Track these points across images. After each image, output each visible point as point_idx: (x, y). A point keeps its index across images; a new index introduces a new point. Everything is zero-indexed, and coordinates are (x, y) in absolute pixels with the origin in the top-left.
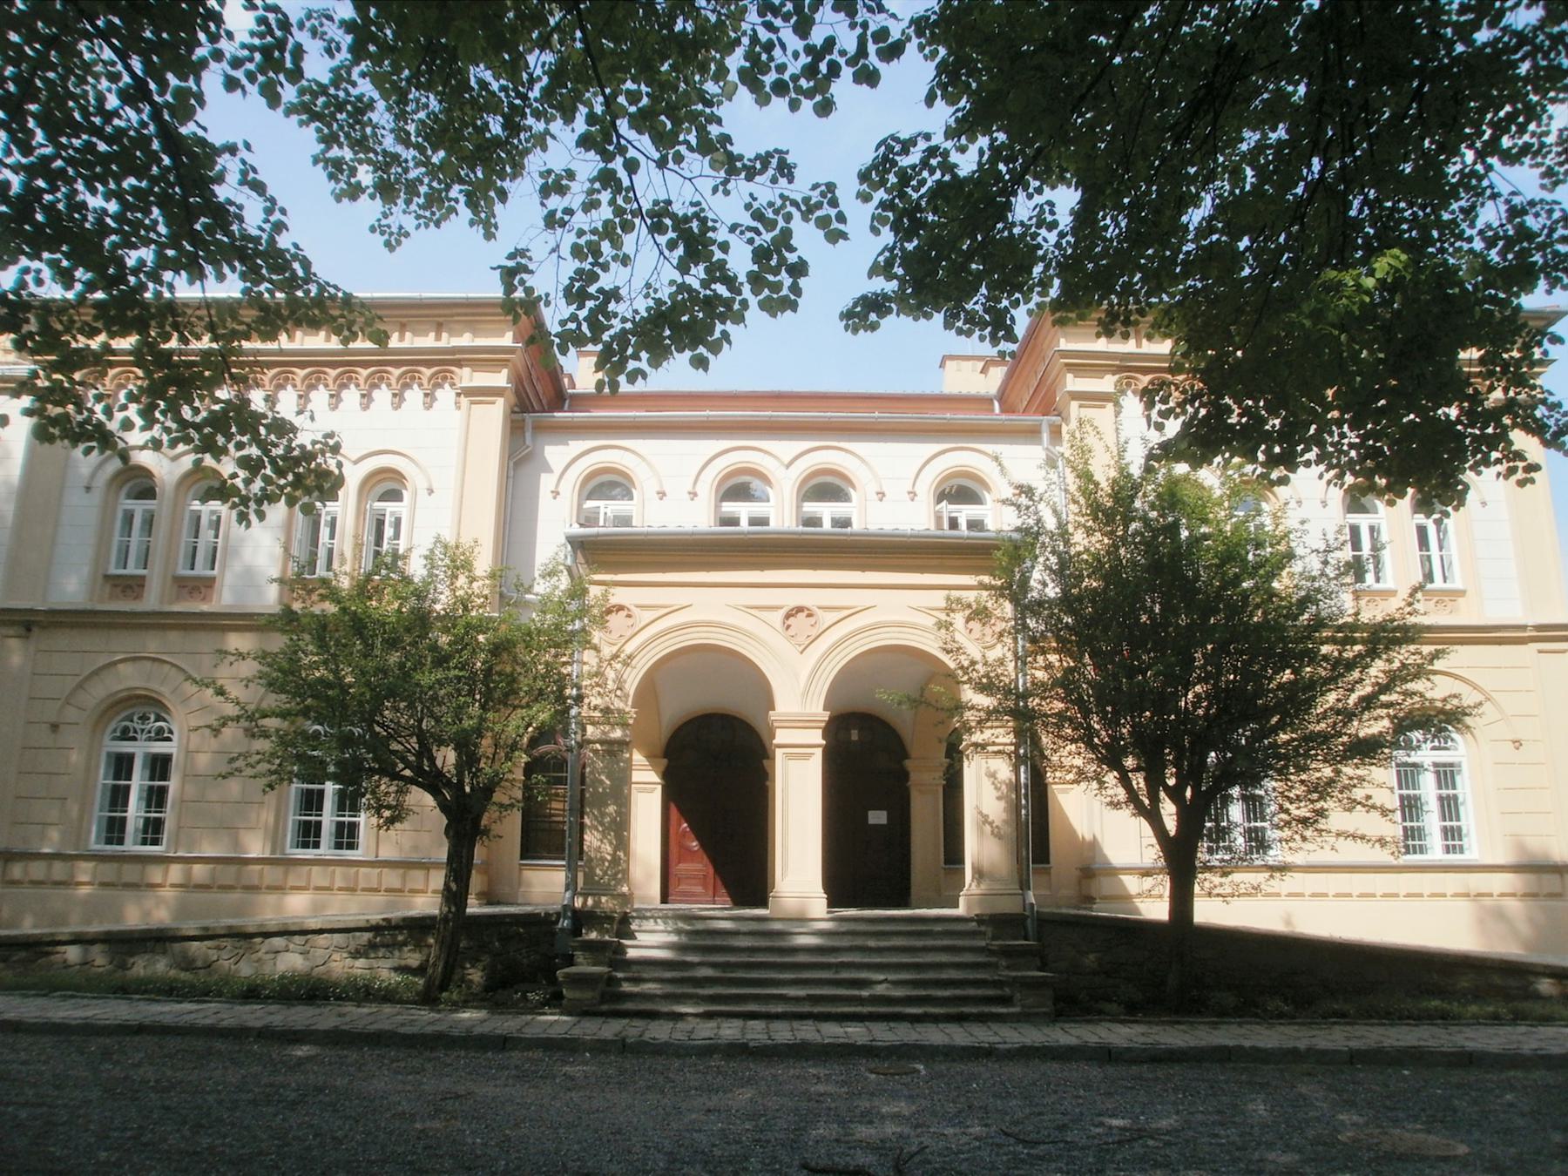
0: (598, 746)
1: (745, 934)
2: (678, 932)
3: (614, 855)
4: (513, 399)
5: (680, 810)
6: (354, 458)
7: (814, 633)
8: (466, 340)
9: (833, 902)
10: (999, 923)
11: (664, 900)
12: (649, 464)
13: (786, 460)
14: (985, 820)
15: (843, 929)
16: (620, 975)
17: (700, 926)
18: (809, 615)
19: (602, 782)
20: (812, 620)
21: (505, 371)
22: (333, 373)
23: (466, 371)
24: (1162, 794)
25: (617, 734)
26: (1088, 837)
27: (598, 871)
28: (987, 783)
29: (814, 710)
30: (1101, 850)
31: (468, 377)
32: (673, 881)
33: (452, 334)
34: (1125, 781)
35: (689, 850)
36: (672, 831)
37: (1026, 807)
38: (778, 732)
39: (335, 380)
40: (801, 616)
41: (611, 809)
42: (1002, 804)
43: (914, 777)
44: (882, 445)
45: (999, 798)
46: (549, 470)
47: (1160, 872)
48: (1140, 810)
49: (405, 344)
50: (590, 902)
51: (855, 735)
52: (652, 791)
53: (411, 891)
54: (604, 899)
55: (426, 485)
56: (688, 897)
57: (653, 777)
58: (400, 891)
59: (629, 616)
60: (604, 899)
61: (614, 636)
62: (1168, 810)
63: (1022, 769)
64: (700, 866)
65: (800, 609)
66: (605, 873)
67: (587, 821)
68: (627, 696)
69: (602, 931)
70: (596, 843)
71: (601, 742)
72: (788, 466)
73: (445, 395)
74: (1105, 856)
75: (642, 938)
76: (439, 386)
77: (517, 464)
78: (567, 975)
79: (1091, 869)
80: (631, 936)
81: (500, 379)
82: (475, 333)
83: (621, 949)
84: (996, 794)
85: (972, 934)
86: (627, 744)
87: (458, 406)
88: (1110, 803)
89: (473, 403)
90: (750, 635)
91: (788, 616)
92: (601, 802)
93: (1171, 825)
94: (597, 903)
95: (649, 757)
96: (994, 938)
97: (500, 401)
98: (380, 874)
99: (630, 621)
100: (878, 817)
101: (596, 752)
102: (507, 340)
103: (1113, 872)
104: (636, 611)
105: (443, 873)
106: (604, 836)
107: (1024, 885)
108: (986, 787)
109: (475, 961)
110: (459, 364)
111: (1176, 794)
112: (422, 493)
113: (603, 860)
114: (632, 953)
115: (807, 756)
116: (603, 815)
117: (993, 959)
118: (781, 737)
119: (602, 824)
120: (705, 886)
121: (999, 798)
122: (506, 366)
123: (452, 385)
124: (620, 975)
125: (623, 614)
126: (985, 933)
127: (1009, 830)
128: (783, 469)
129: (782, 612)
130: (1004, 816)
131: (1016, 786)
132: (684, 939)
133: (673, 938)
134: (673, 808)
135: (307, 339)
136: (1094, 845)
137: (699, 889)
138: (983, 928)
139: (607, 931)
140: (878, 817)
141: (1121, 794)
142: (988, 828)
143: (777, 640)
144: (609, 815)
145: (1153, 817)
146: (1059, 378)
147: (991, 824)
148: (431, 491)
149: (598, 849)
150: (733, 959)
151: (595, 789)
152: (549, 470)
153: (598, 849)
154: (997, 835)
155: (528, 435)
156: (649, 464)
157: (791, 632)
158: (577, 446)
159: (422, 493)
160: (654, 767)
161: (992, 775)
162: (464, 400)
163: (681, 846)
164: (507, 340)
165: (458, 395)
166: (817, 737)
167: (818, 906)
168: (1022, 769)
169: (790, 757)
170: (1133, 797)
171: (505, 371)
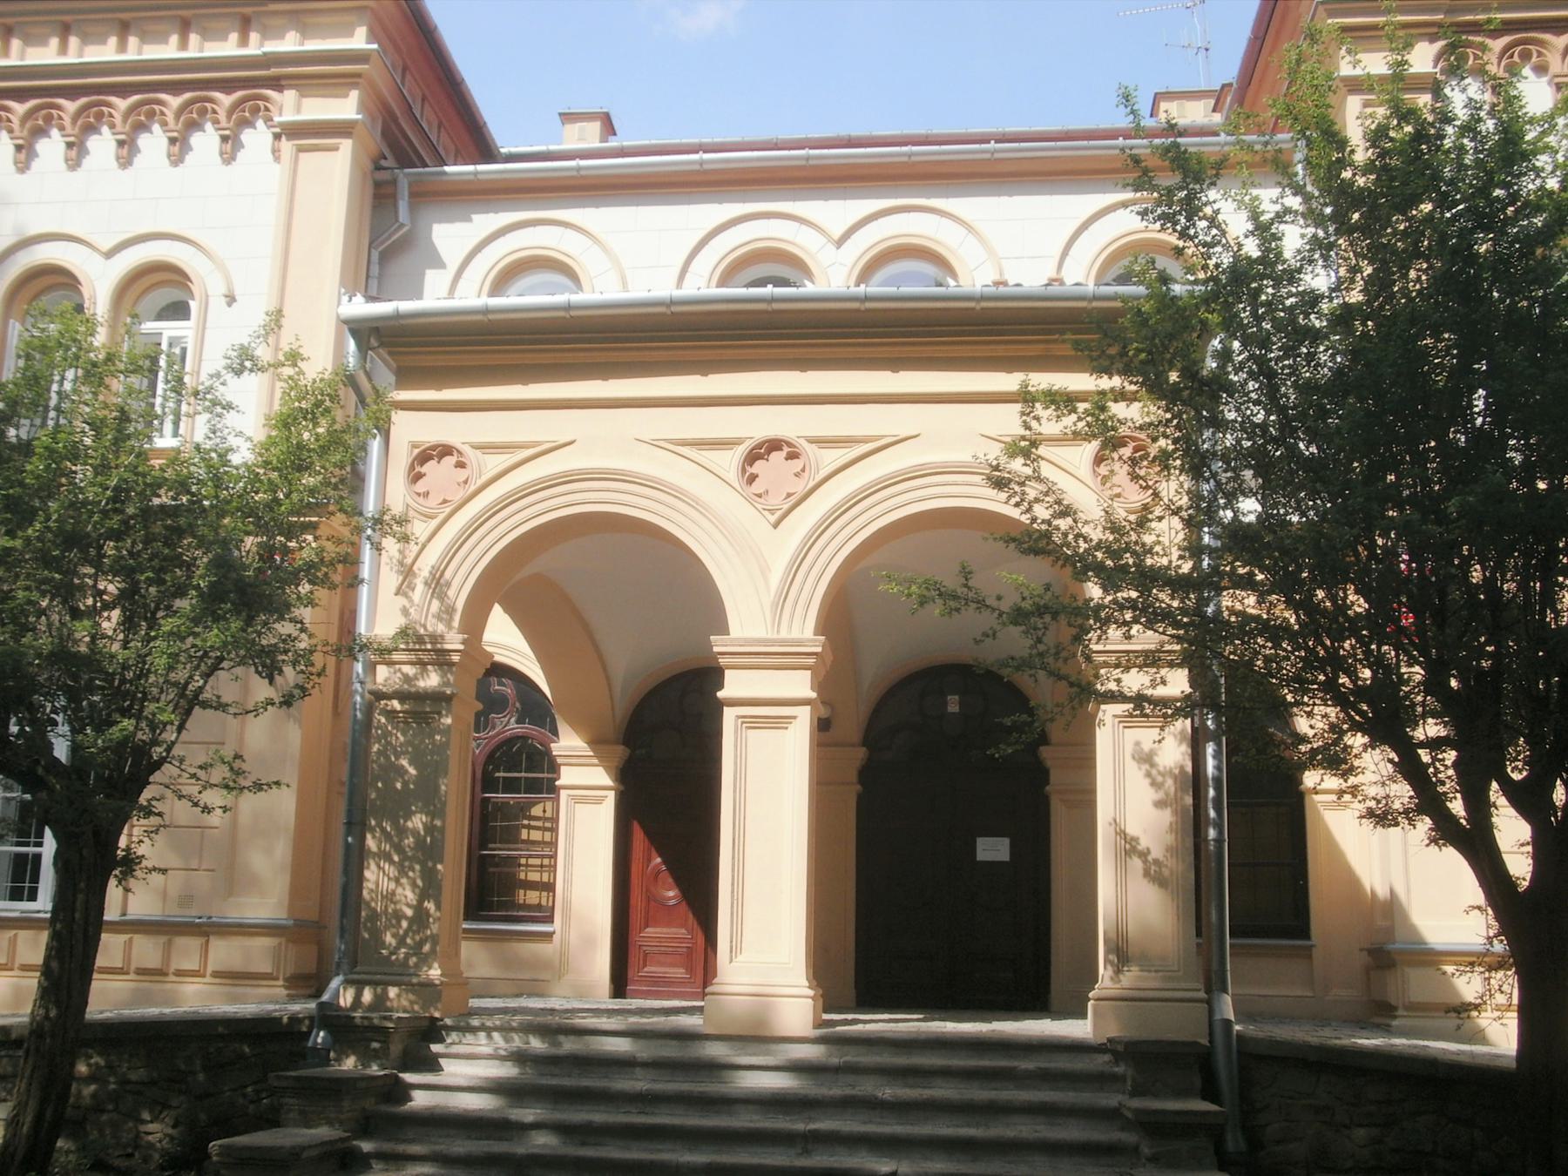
0: (396, 704)
1: (646, 1065)
2: (520, 1058)
3: (419, 909)
4: (375, 143)
5: (649, 834)
6: (106, 246)
7: (800, 487)
8: (289, 43)
9: (829, 1000)
10: (1144, 1059)
11: (620, 984)
12: (605, 249)
13: (837, 233)
14: (1128, 847)
15: (835, 1061)
16: (367, 1146)
17: (569, 1045)
18: (793, 456)
19: (401, 771)
20: (796, 465)
21: (354, 95)
22: (70, 106)
23: (290, 95)
24: (1495, 791)
25: (432, 680)
26: (1382, 892)
27: (389, 939)
28: (1136, 778)
29: (795, 634)
30: (1405, 917)
31: (290, 106)
32: (634, 958)
33: (266, 35)
34: (1409, 768)
35: (662, 904)
36: (635, 869)
37: (1218, 826)
38: (729, 675)
39: (75, 119)
40: (777, 457)
41: (418, 822)
42: (1166, 816)
43: (1055, 776)
44: (1004, 199)
45: (1159, 804)
46: (439, 264)
47: (169, 944)
48: (1447, 832)
49: (192, 53)
50: (367, 996)
51: (953, 705)
52: (599, 801)
53: (179, 973)
54: (393, 992)
55: (224, 290)
56: (660, 986)
57: (600, 777)
58: (160, 973)
59: (461, 465)
60: (393, 992)
61: (433, 501)
62: (1512, 832)
63: (1210, 749)
64: (682, 932)
65: (774, 445)
66: (401, 942)
67: (371, 843)
68: (450, 611)
69: (366, 1057)
70: (387, 885)
71: (401, 696)
72: (840, 242)
73: (257, 138)
74: (1413, 930)
75: (455, 1070)
76: (247, 123)
77: (385, 257)
78: (226, 1150)
79: (1388, 951)
80: (432, 1064)
81: (346, 107)
82: (306, 32)
83: (401, 1092)
84: (1151, 795)
85: (1100, 1080)
86: (448, 699)
87: (276, 152)
88: (1370, 814)
89: (301, 149)
90: (677, 493)
91: (753, 457)
92: (397, 807)
93: (1520, 866)
94: (380, 1002)
95: (596, 742)
96: (1136, 1092)
97: (346, 145)
98: (13, 942)
99: (462, 474)
100: (993, 849)
101: (391, 714)
102: (359, 40)
103: (1430, 958)
104: (471, 455)
105: (44, 936)
106: (402, 871)
107: (1214, 982)
108: (1134, 778)
109: (159, 1107)
110: (277, 84)
111: (1529, 800)
112: (217, 303)
113: (399, 916)
114: (420, 1100)
115: (781, 723)
116: (402, 832)
117: (1129, 1138)
118: (734, 685)
119: (399, 849)
120: (690, 969)
121: (1159, 804)
122: (354, 86)
123: (268, 120)
124: (367, 1146)
125: (450, 461)
126: (1123, 1078)
127: (1179, 868)
128: (832, 248)
129: (740, 451)
130: (1170, 839)
131: (1196, 780)
132: (531, 1075)
133: (507, 1071)
134: (639, 837)
135: (31, 51)
136: (1391, 908)
137: (679, 972)
138: (1120, 1069)
139: (375, 1056)
140: (993, 849)
141: (1402, 793)
142: (1136, 863)
143: (730, 502)
144: (415, 833)
145: (1476, 844)
146: (1327, 58)
147: (1144, 855)
148: (231, 299)
149: (390, 897)
150: (598, 1116)
151: (389, 784)
152: (439, 264)
153: (390, 897)
154: (1155, 875)
155: (403, 206)
156: (605, 249)
157: (758, 487)
158: (486, 222)
159: (217, 303)
160: (603, 759)
161: (1146, 759)
162: (287, 146)
163: (650, 898)
164: (359, 40)
165: (277, 137)
166: (800, 685)
167: (795, 1008)
168: (1210, 749)
169: (755, 723)
170: (1429, 801)
171: (354, 95)
